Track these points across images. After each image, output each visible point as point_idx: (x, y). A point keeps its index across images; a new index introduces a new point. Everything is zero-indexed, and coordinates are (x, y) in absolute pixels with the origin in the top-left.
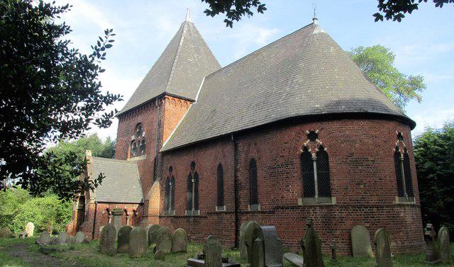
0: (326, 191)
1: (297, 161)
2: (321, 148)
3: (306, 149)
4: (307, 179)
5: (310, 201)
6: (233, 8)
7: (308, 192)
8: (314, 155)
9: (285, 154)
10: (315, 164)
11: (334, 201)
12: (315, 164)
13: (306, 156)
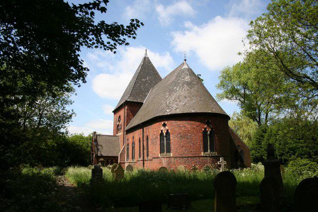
0: (169, 151)
2: (167, 130)
4: (162, 145)
7: (162, 151)
11: (171, 155)
13: (162, 134)
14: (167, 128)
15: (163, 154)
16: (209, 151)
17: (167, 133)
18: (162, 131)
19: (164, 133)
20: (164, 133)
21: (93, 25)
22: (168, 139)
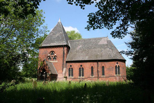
0: (119, 73)
1: (115, 68)
2: (119, 65)
3: (116, 65)
4: (116, 71)
5: (80, 77)
6: (2, 81)
7: (116, 74)
8: (117, 67)
9: (112, 66)
10: (117, 69)
11: (94, 76)
12: (117, 69)
13: (116, 67)
14: (118, 64)
15: (117, 75)
16: (81, 76)
17: (119, 67)
18: (116, 65)
19: (117, 66)
20: (117, 66)
21: (136, 1)
22: (119, 69)
